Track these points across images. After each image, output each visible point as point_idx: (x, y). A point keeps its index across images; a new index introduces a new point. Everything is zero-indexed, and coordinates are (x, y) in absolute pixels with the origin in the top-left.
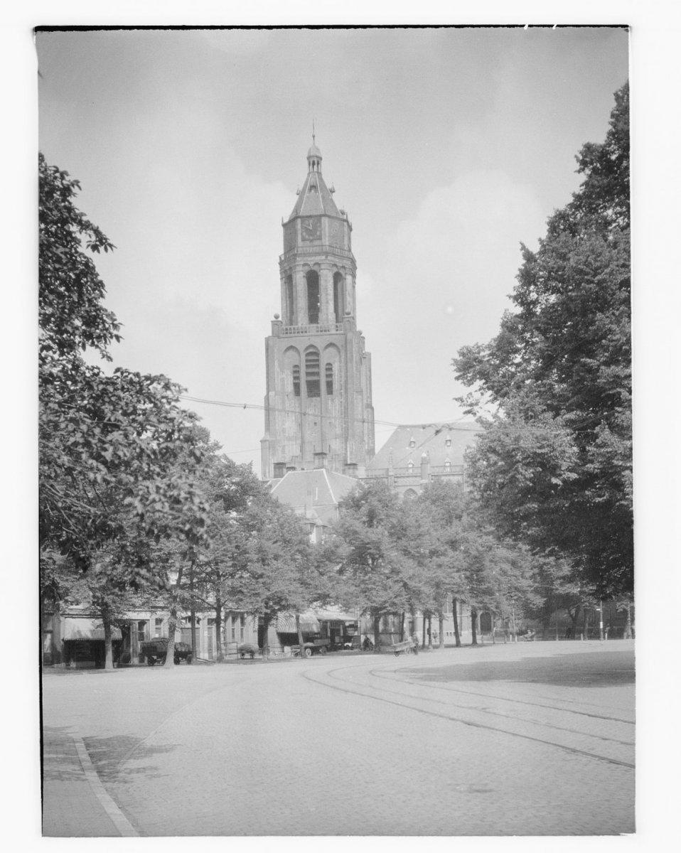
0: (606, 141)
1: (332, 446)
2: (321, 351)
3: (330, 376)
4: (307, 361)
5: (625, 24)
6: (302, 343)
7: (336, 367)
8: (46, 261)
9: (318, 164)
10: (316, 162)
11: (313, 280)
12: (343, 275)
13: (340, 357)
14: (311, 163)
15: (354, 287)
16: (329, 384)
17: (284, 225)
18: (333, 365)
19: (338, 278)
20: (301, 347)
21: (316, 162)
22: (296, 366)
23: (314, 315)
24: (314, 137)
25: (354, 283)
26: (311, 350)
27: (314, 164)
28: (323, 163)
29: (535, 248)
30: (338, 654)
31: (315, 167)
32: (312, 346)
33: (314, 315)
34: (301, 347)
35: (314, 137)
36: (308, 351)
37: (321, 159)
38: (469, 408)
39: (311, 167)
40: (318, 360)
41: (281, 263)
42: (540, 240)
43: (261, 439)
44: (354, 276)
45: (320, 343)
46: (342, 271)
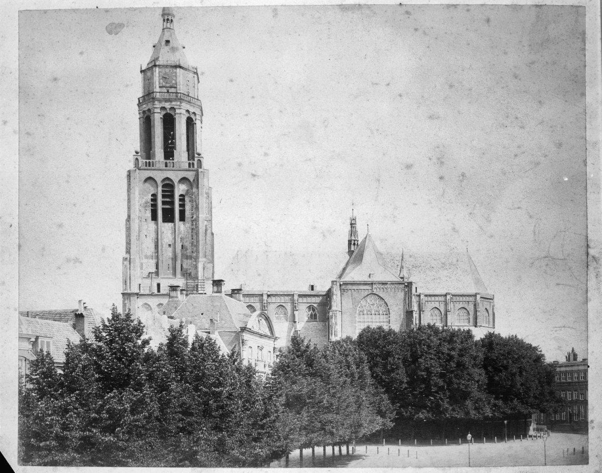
0: (506, 338)
2: (176, 184)
4: (163, 191)
5: (347, 243)
6: (159, 176)
8: (62, 443)
11: (169, 121)
12: (194, 119)
16: (182, 213)
19: (190, 123)
20: (159, 180)
23: (169, 153)
26: (168, 182)
32: (168, 179)
33: (169, 153)
34: (159, 180)
36: (166, 182)
43: (152, 193)
45: (175, 177)
46: (193, 116)
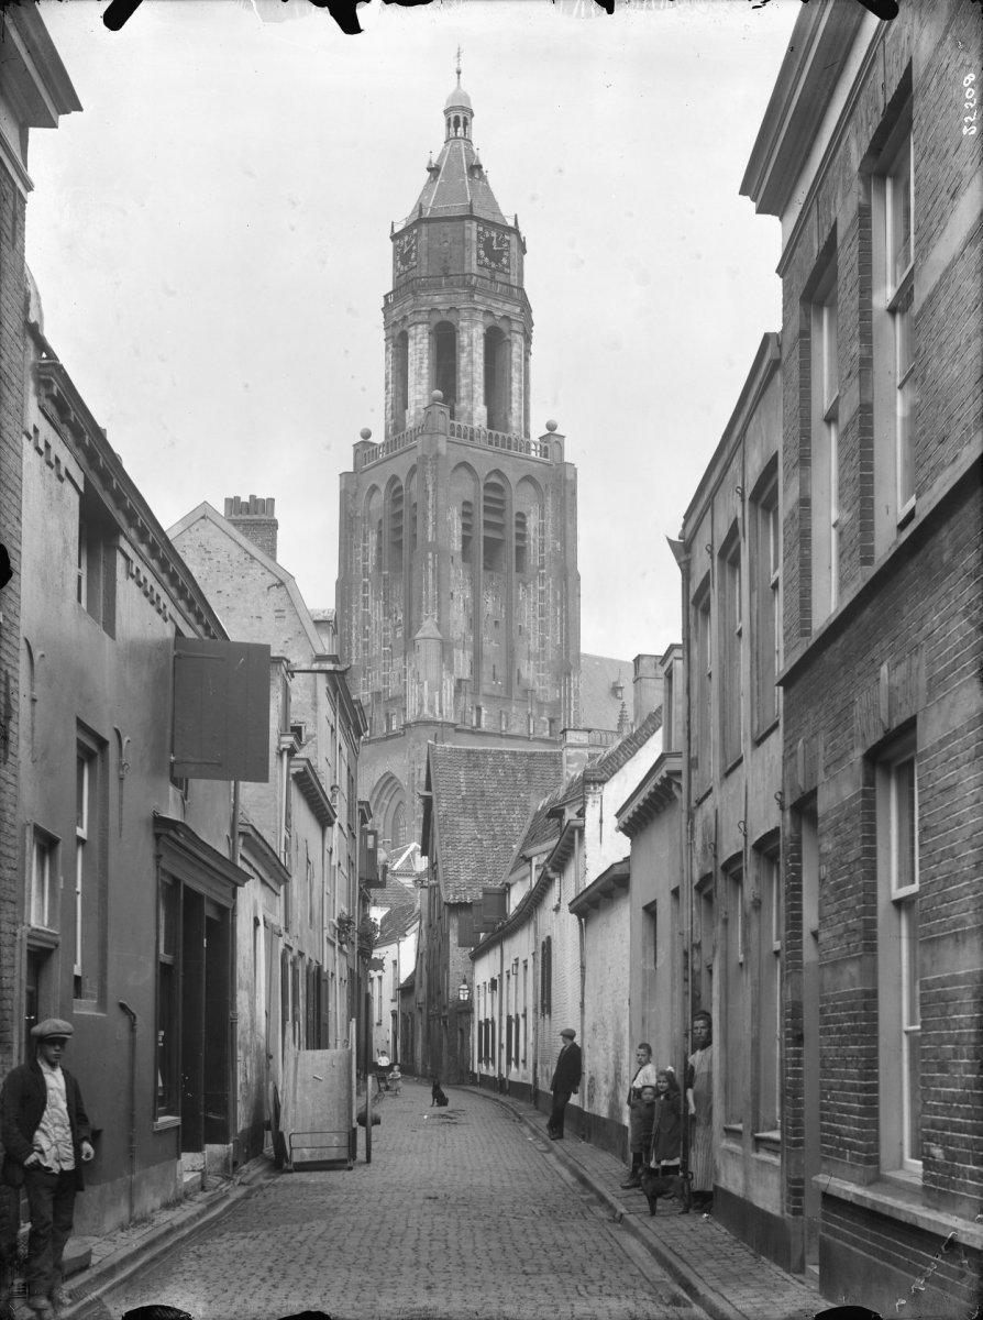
1: (522, 672)
3: (521, 537)
7: (532, 522)
9: (466, 124)
10: (461, 120)
13: (542, 507)
14: (452, 120)
15: (527, 360)
17: (394, 237)
18: (528, 518)
19: (495, 341)
21: (461, 120)
22: (466, 504)
24: (459, 73)
25: (528, 352)
27: (457, 124)
28: (475, 122)
29: (675, 538)
30: (644, 938)
31: (460, 129)
32: (497, 472)
34: (483, 471)
35: (459, 73)
37: (472, 115)
38: (916, 306)
39: (452, 129)
40: (501, 502)
41: (387, 308)
42: (671, 542)
44: (528, 340)
